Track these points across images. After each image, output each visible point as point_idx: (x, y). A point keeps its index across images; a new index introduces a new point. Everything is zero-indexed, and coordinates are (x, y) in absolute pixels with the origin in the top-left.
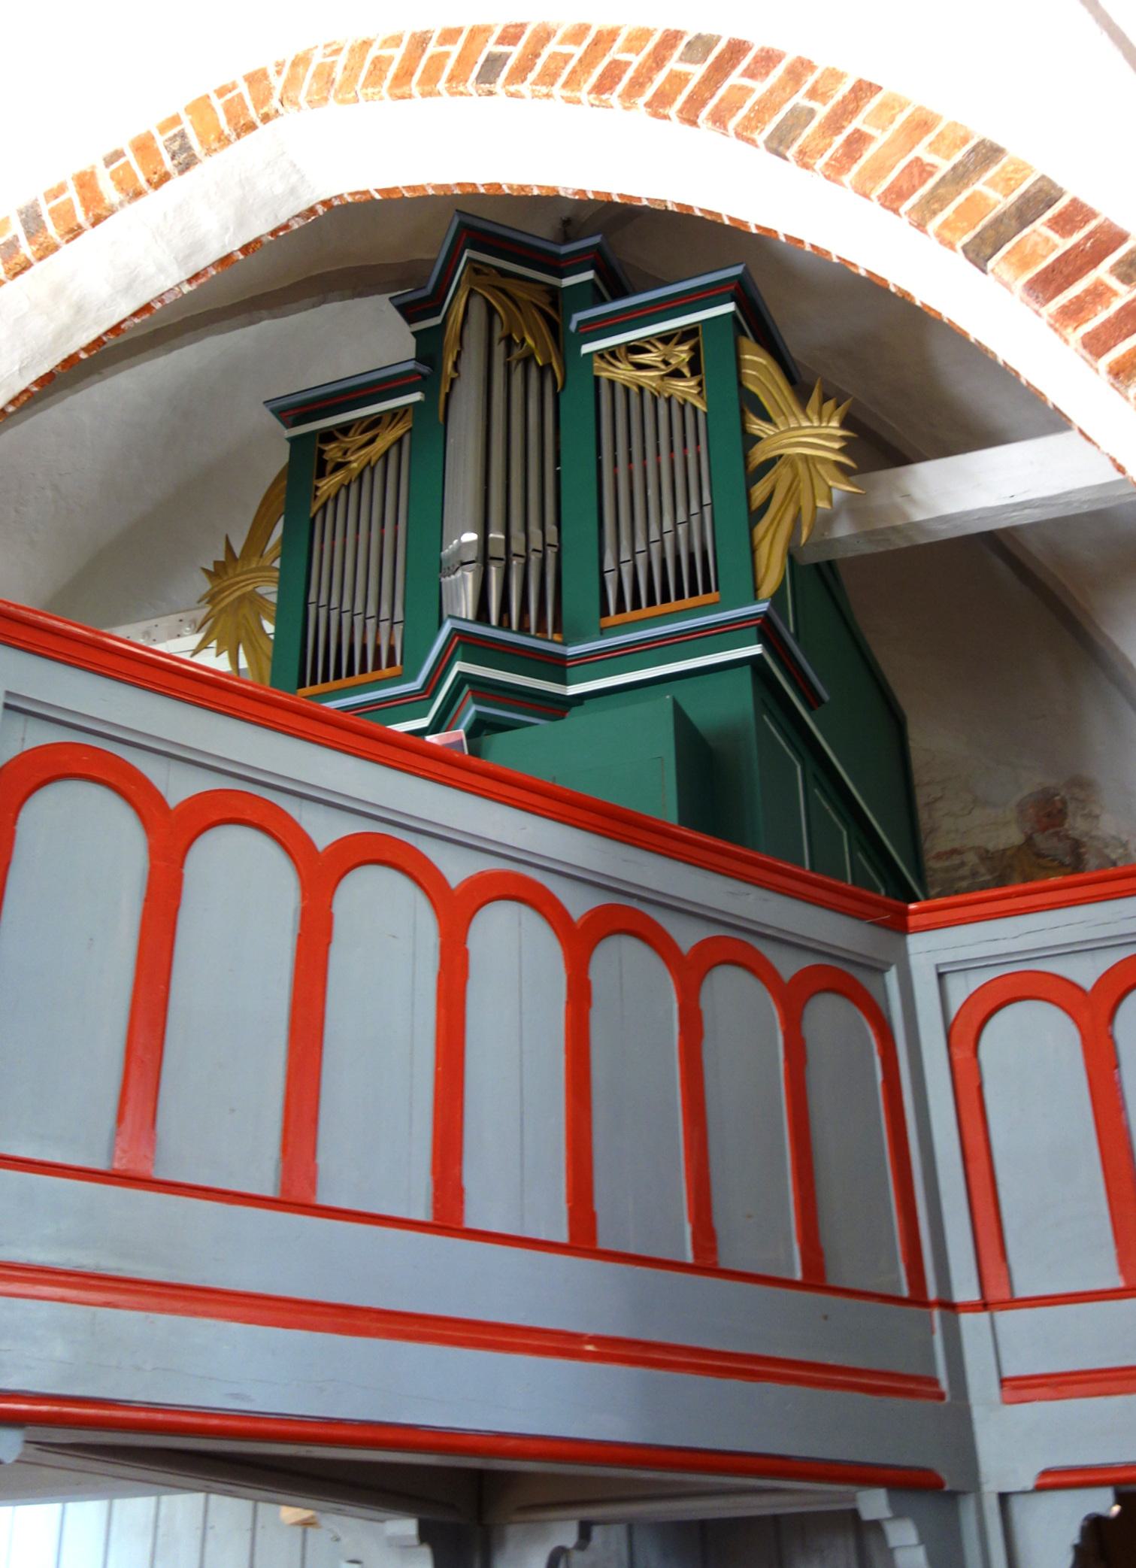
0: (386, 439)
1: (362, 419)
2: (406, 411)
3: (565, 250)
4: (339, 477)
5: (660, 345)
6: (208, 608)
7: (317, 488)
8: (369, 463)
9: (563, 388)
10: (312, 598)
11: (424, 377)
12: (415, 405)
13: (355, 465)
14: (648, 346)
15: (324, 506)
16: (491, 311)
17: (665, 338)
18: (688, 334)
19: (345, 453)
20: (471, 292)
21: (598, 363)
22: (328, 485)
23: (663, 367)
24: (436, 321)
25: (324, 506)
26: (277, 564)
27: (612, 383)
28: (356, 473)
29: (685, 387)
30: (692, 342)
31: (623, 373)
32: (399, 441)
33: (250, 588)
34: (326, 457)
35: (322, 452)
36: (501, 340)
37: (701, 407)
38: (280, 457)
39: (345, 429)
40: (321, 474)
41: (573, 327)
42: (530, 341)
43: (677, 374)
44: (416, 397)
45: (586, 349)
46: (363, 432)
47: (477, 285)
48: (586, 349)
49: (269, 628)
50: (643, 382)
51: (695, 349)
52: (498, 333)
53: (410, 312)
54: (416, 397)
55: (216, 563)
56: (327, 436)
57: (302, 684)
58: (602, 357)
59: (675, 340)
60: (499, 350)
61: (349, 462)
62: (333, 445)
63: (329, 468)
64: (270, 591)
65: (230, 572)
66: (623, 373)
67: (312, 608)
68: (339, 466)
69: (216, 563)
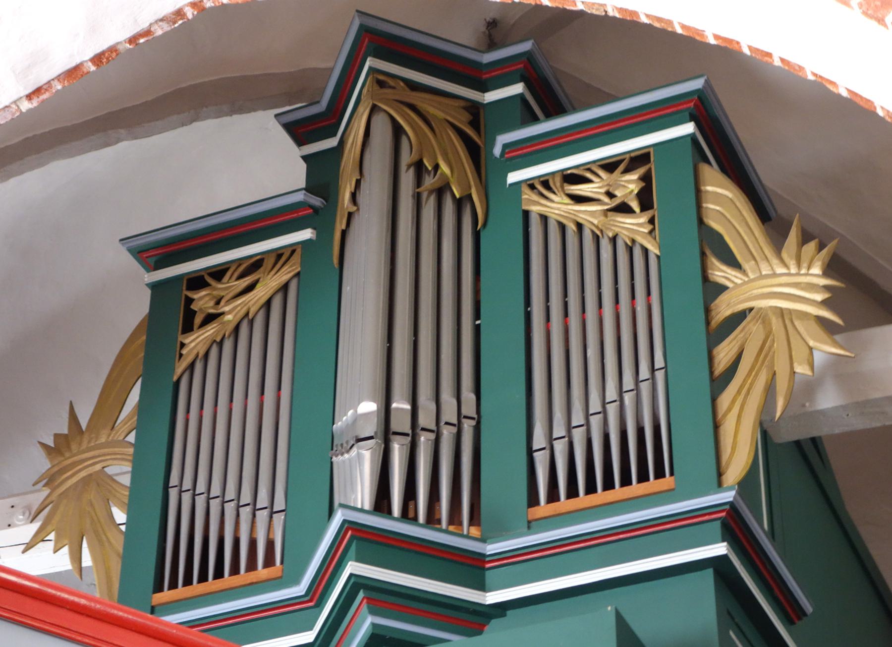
0: (269, 284)
1: (240, 261)
2: (293, 252)
3: (488, 58)
4: (210, 331)
5: (601, 173)
6: (46, 491)
7: (183, 345)
8: (247, 314)
9: (485, 224)
10: (174, 480)
11: (316, 210)
12: (304, 243)
13: (229, 317)
14: (589, 175)
15: (192, 366)
16: (398, 131)
17: (610, 166)
18: (639, 159)
19: (218, 303)
20: (374, 109)
21: (527, 195)
22: (196, 342)
23: (606, 199)
24: (332, 142)
25: (192, 366)
26: (131, 438)
27: (544, 219)
28: (231, 327)
29: (633, 225)
30: (642, 171)
31: (558, 207)
32: (285, 288)
33: (98, 467)
34: (194, 307)
35: (189, 301)
36: (409, 166)
37: (653, 249)
38: (139, 306)
39: (218, 273)
40: (188, 328)
41: (497, 151)
42: (444, 168)
43: (623, 209)
44: (306, 234)
45: (513, 177)
46: (241, 277)
47: (381, 100)
48: (513, 177)
49: (120, 516)
50: (582, 218)
51: (646, 179)
52: (406, 158)
53: (300, 131)
54: (306, 234)
55: (57, 436)
56: (197, 282)
57: (158, 588)
58: (532, 187)
59: (622, 167)
60: (407, 178)
61: (223, 314)
62: (203, 293)
63: (198, 320)
64: (121, 472)
65: (74, 447)
66: (558, 207)
67: (173, 494)
68: (210, 318)
69: (57, 436)
